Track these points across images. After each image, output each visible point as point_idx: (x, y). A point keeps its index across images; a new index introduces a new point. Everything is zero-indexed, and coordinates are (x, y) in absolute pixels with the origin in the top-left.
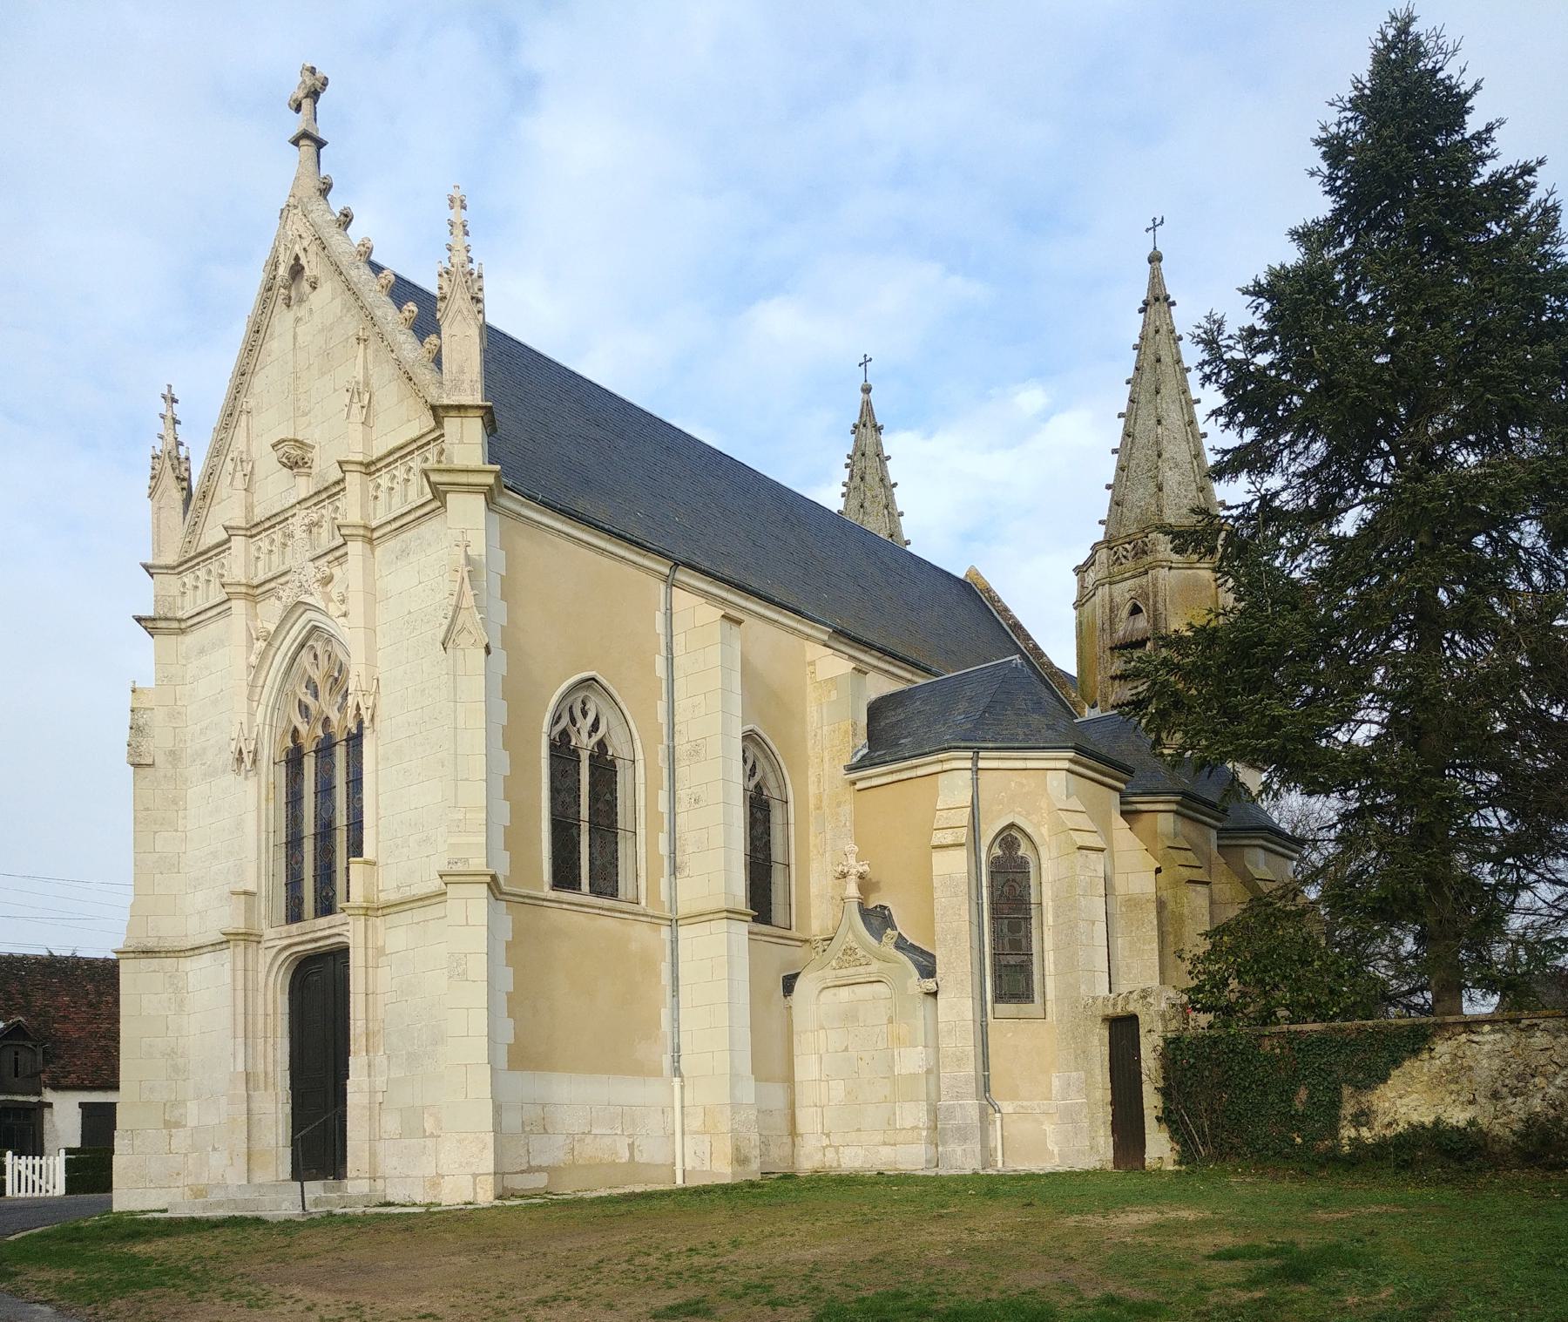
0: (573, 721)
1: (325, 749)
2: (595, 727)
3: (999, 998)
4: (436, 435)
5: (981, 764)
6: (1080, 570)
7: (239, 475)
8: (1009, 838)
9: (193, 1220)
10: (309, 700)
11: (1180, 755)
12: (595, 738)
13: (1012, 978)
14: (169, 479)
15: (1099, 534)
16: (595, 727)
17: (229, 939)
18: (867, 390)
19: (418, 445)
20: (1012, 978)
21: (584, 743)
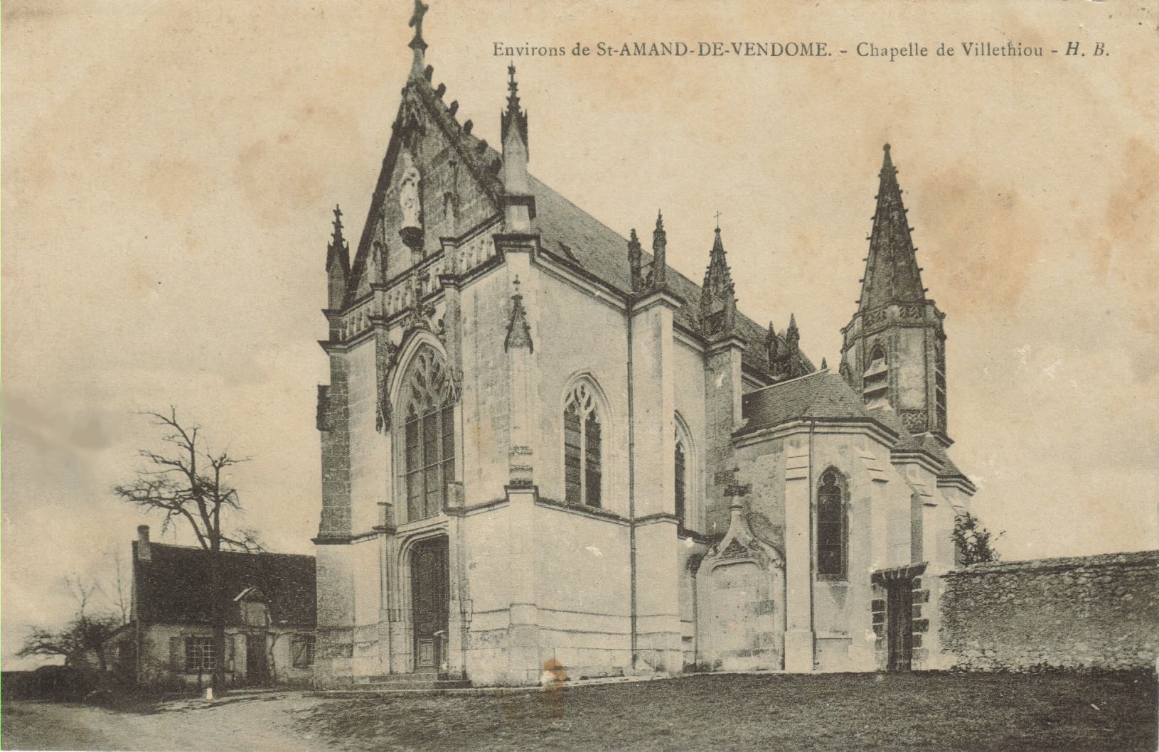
0: (577, 399)
1: (429, 418)
2: (589, 403)
3: (821, 571)
4: (500, 216)
5: (816, 430)
6: (845, 331)
7: (379, 253)
8: (831, 474)
9: (385, 162)
10: (420, 388)
11: (229, 672)
12: (590, 409)
13: (831, 558)
14: (337, 261)
15: (855, 308)
16: (589, 403)
17: (378, 530)
18: (718, 231)
19: (487, 223)
20: (831, 558)
21: (584, 414)
